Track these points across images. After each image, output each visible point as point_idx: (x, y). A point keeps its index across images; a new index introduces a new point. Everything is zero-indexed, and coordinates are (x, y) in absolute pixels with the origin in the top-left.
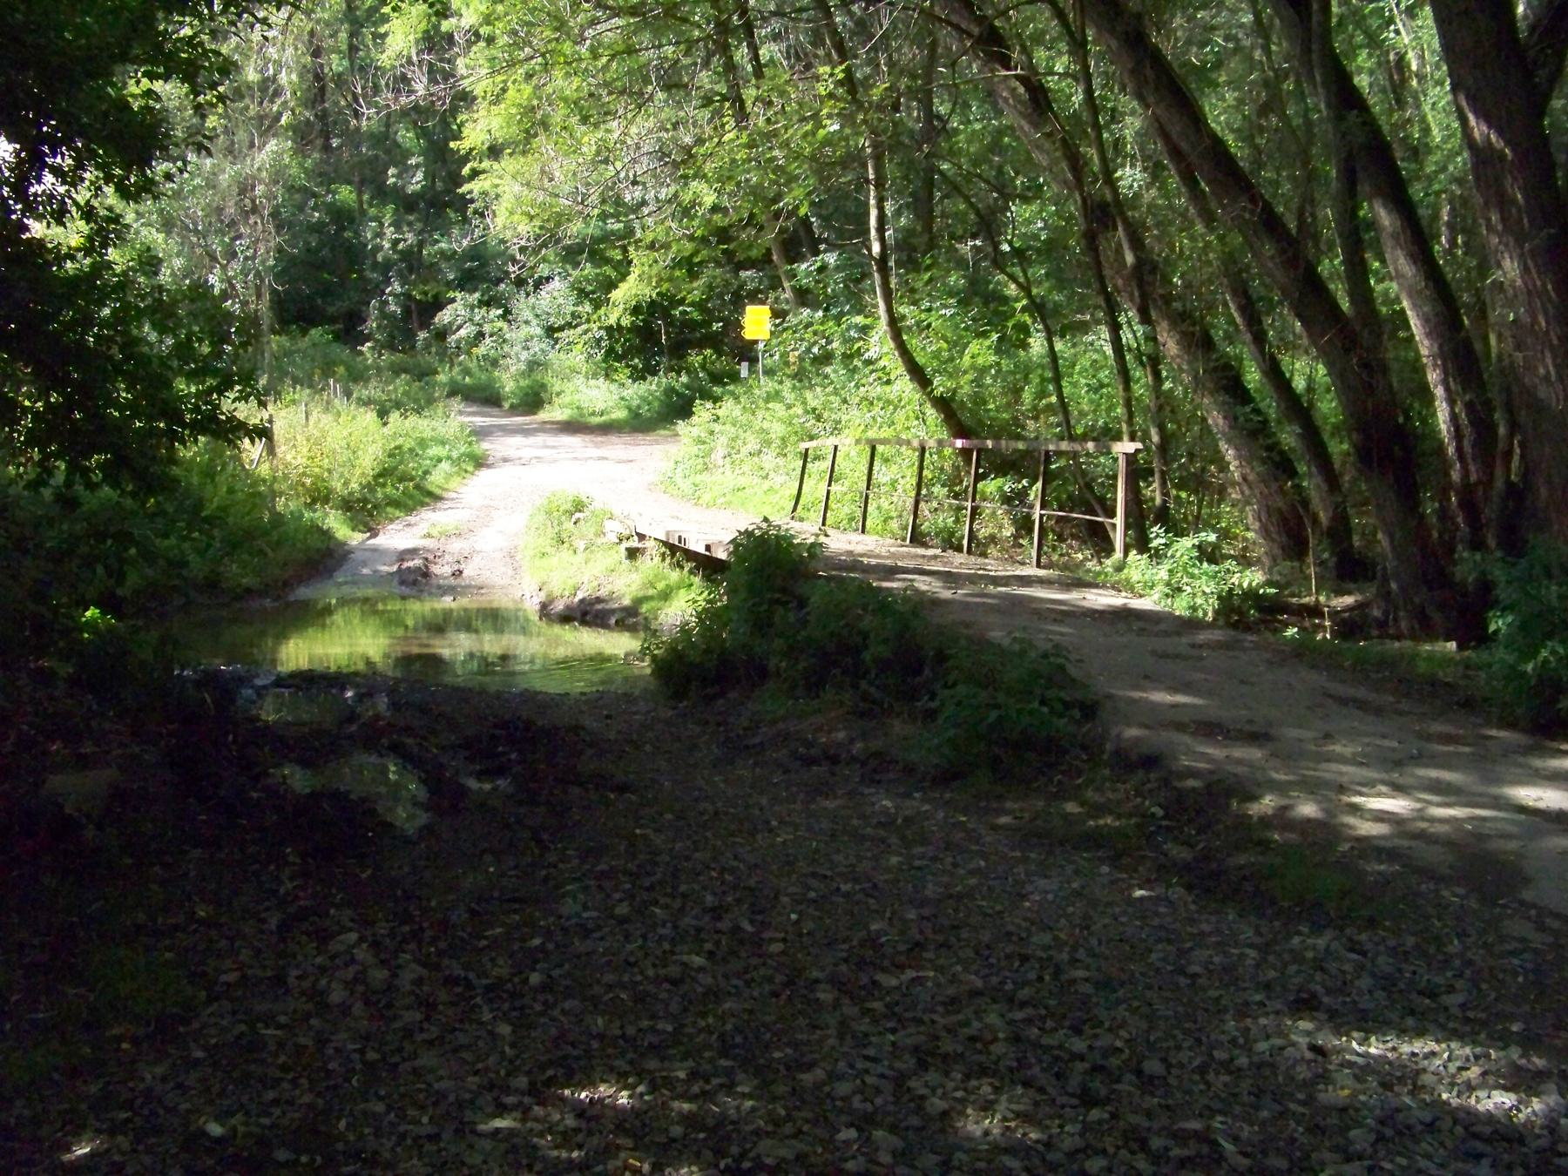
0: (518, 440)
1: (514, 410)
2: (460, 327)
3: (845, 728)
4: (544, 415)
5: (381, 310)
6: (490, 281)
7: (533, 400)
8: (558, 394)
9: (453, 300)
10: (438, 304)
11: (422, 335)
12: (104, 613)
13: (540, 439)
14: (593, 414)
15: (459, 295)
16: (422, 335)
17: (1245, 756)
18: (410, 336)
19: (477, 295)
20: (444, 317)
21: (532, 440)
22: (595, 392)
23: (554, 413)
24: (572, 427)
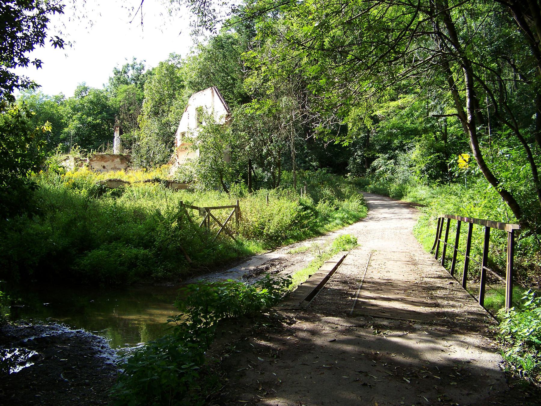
0: (386, 210)
1: (394, 198)
2: (380, 167)
3: (221, 251)
4: (403, 200)
5: (354, 161)
6: (392, 150)
7: (399, 195)
8: (409, 192)
9: (379, 157)
10: (374, 158)
11: (368, 170)
12: (41, 130)
13: (396, 210)
14: (420, 200)
15: (380, 155)
16: (368, 170)
17: (426, 308)
18: (364, 171)
19: (387, 155)
20: (375, 163)
21: (392, 210)
22: (423, 192)
23: (407, 200)
24: (409, 206)
